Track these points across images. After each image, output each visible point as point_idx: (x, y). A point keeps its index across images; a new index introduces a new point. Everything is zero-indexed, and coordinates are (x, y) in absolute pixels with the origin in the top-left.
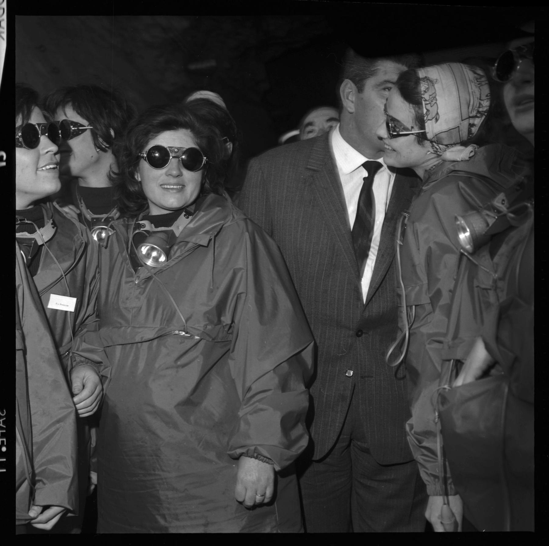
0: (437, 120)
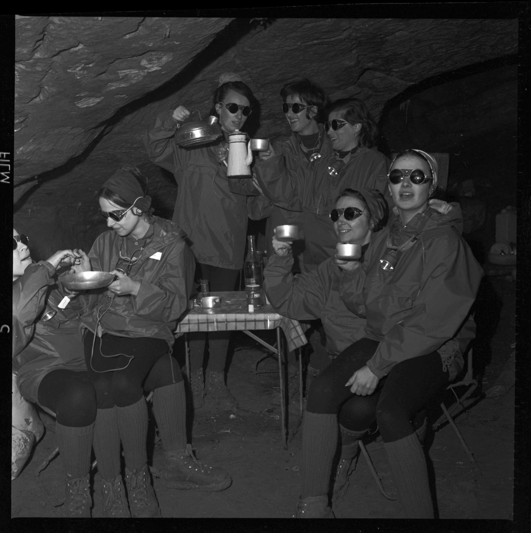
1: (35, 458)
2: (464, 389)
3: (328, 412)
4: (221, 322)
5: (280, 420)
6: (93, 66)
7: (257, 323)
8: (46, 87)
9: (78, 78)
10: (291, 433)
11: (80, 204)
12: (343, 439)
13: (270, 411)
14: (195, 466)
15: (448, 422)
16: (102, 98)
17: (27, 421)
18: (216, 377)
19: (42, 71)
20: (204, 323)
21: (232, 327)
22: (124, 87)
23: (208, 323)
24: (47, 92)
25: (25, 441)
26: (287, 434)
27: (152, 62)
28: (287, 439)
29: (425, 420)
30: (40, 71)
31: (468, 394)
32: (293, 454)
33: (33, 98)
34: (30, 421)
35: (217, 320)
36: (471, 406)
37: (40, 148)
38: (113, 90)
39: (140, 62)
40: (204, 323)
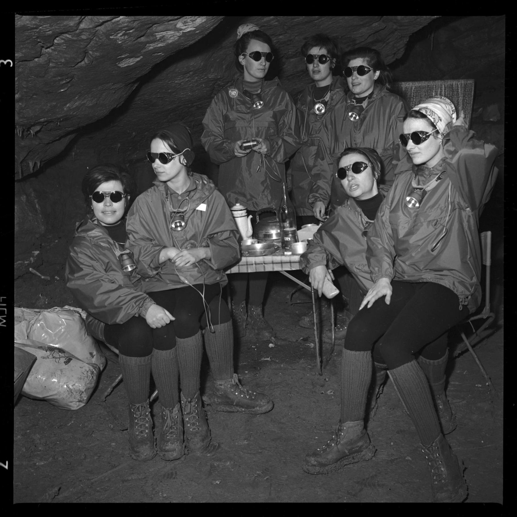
0: (441, 120)
1: (100, 386)
2: (482, 321)
3: (364, 350)
4: (259, 264)
5: (315, 348)
6: (133, 32)
7: (292, 264)
8: (90, 52)
9: (120, 42)
10: (324, 360)
11: (119, 145)
13: (306, 340)
14: (241, 392)
15: (467, 350)
16: (142, 57)
17: (91, 354)
18: (256, 311)
19: (87, 39)
20: (244, 265)
21: (269, 268)
22: (161, 47)
23: (247, 265)
24: (92, 56)
25: (92, 373)
26: (321, 362)
27: (187, 24)
28: (321, 366)
29: (447, 350)
30: (85, 40)
31: (486, 325)
32: (327, 380)
33: (78, 63)
34: (94, 354)
35: (255, 262)
36: (488, 337)
37: (84, 104)
38: (151, 50)
39: (176, 25)
40: (244, 265)
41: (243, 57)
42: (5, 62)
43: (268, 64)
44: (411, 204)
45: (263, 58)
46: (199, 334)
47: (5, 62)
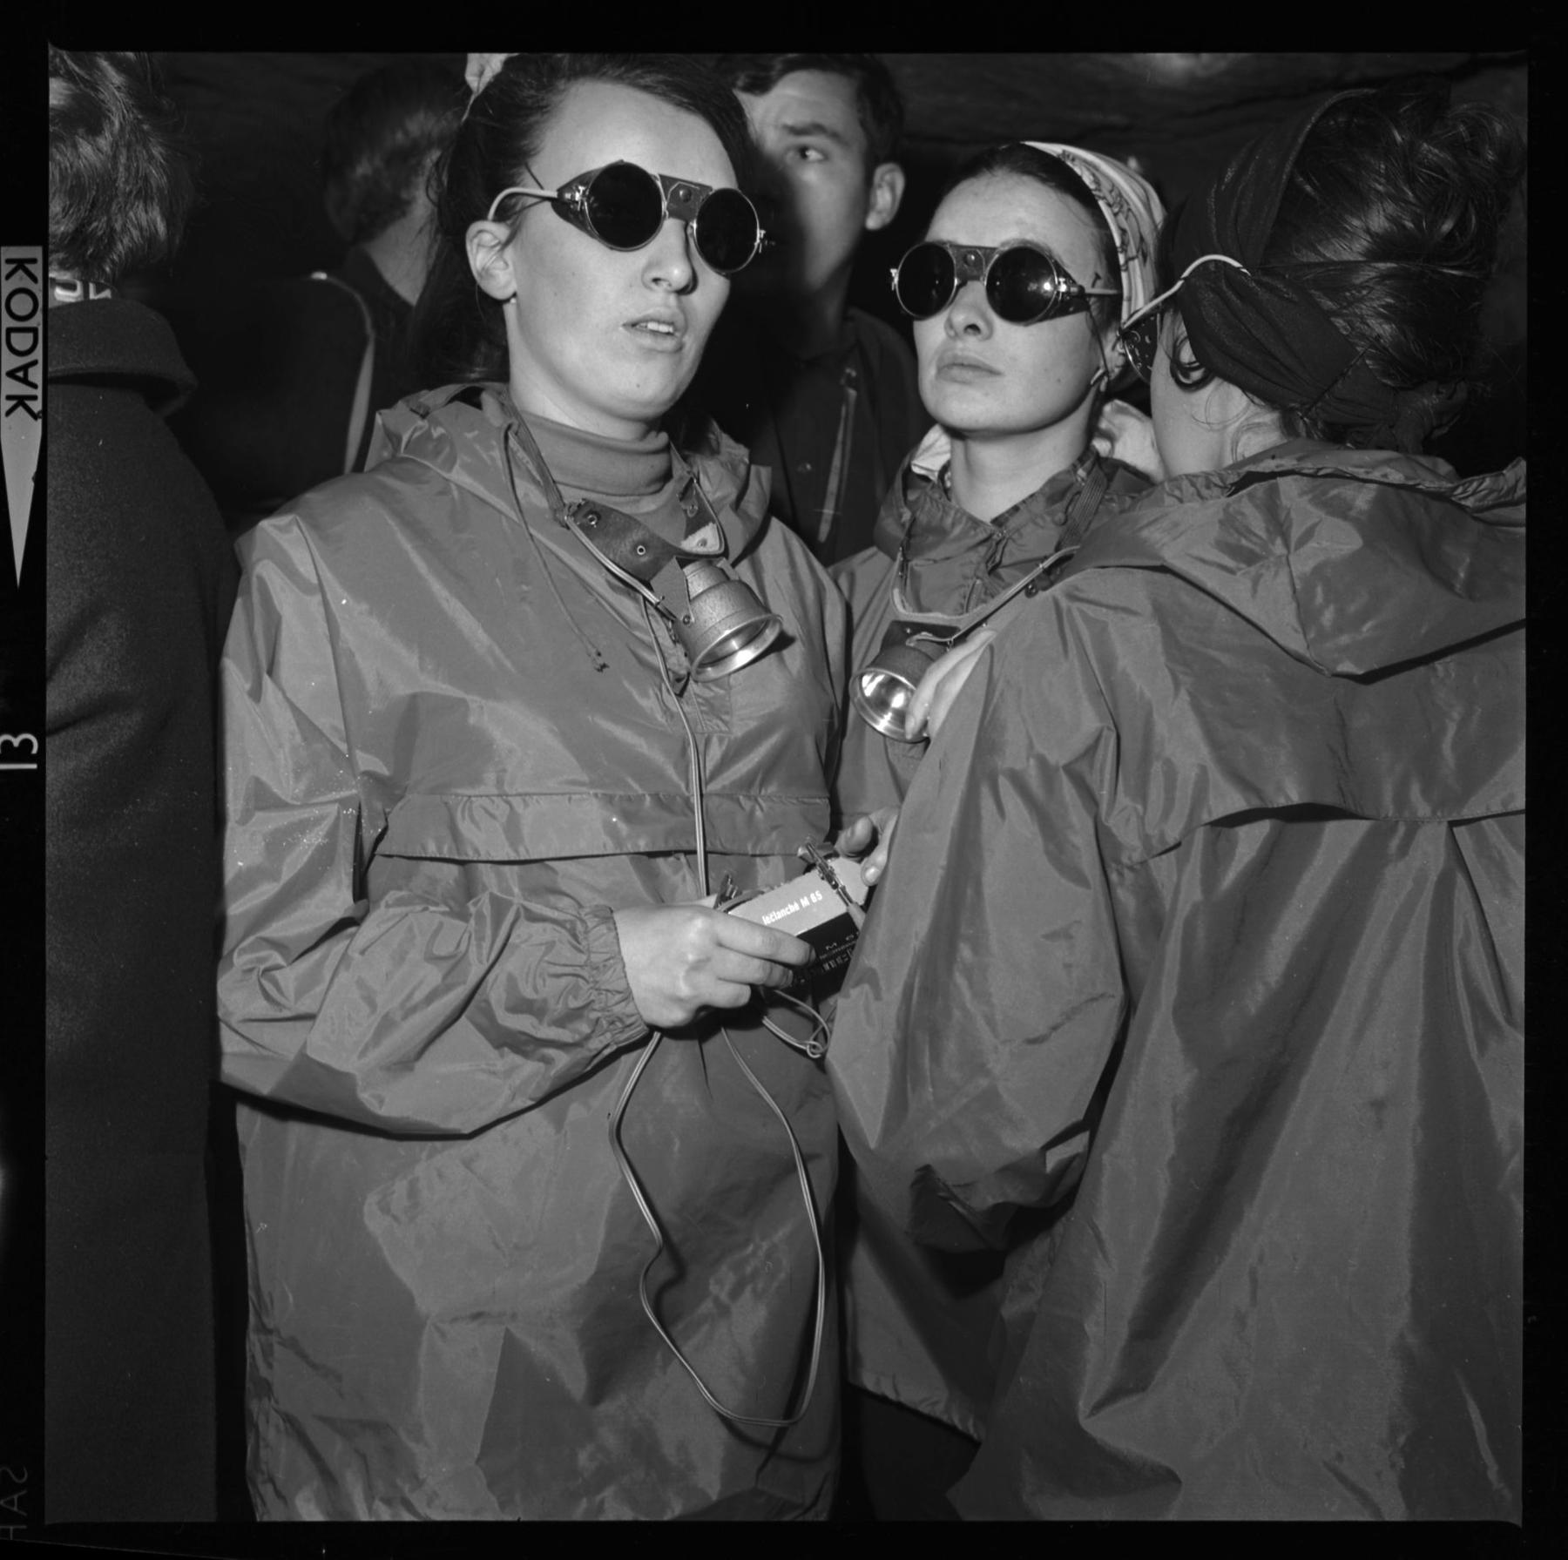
12: (1256, 803)
41: (501, 231)
42: (16, 742)
43: (713, 288)
44: (888, 716)
45: (670, 233)
46: (243, 1114)
47: (16, 742)
